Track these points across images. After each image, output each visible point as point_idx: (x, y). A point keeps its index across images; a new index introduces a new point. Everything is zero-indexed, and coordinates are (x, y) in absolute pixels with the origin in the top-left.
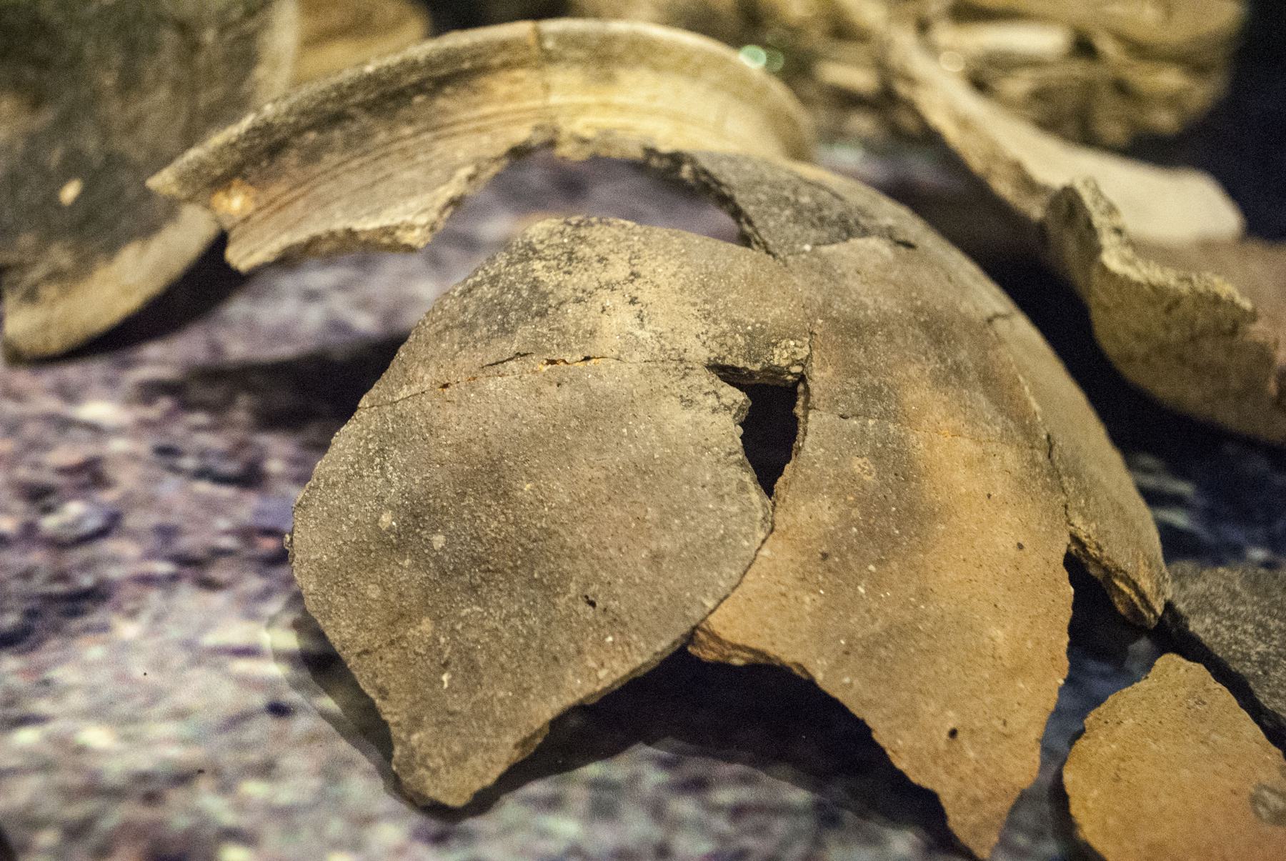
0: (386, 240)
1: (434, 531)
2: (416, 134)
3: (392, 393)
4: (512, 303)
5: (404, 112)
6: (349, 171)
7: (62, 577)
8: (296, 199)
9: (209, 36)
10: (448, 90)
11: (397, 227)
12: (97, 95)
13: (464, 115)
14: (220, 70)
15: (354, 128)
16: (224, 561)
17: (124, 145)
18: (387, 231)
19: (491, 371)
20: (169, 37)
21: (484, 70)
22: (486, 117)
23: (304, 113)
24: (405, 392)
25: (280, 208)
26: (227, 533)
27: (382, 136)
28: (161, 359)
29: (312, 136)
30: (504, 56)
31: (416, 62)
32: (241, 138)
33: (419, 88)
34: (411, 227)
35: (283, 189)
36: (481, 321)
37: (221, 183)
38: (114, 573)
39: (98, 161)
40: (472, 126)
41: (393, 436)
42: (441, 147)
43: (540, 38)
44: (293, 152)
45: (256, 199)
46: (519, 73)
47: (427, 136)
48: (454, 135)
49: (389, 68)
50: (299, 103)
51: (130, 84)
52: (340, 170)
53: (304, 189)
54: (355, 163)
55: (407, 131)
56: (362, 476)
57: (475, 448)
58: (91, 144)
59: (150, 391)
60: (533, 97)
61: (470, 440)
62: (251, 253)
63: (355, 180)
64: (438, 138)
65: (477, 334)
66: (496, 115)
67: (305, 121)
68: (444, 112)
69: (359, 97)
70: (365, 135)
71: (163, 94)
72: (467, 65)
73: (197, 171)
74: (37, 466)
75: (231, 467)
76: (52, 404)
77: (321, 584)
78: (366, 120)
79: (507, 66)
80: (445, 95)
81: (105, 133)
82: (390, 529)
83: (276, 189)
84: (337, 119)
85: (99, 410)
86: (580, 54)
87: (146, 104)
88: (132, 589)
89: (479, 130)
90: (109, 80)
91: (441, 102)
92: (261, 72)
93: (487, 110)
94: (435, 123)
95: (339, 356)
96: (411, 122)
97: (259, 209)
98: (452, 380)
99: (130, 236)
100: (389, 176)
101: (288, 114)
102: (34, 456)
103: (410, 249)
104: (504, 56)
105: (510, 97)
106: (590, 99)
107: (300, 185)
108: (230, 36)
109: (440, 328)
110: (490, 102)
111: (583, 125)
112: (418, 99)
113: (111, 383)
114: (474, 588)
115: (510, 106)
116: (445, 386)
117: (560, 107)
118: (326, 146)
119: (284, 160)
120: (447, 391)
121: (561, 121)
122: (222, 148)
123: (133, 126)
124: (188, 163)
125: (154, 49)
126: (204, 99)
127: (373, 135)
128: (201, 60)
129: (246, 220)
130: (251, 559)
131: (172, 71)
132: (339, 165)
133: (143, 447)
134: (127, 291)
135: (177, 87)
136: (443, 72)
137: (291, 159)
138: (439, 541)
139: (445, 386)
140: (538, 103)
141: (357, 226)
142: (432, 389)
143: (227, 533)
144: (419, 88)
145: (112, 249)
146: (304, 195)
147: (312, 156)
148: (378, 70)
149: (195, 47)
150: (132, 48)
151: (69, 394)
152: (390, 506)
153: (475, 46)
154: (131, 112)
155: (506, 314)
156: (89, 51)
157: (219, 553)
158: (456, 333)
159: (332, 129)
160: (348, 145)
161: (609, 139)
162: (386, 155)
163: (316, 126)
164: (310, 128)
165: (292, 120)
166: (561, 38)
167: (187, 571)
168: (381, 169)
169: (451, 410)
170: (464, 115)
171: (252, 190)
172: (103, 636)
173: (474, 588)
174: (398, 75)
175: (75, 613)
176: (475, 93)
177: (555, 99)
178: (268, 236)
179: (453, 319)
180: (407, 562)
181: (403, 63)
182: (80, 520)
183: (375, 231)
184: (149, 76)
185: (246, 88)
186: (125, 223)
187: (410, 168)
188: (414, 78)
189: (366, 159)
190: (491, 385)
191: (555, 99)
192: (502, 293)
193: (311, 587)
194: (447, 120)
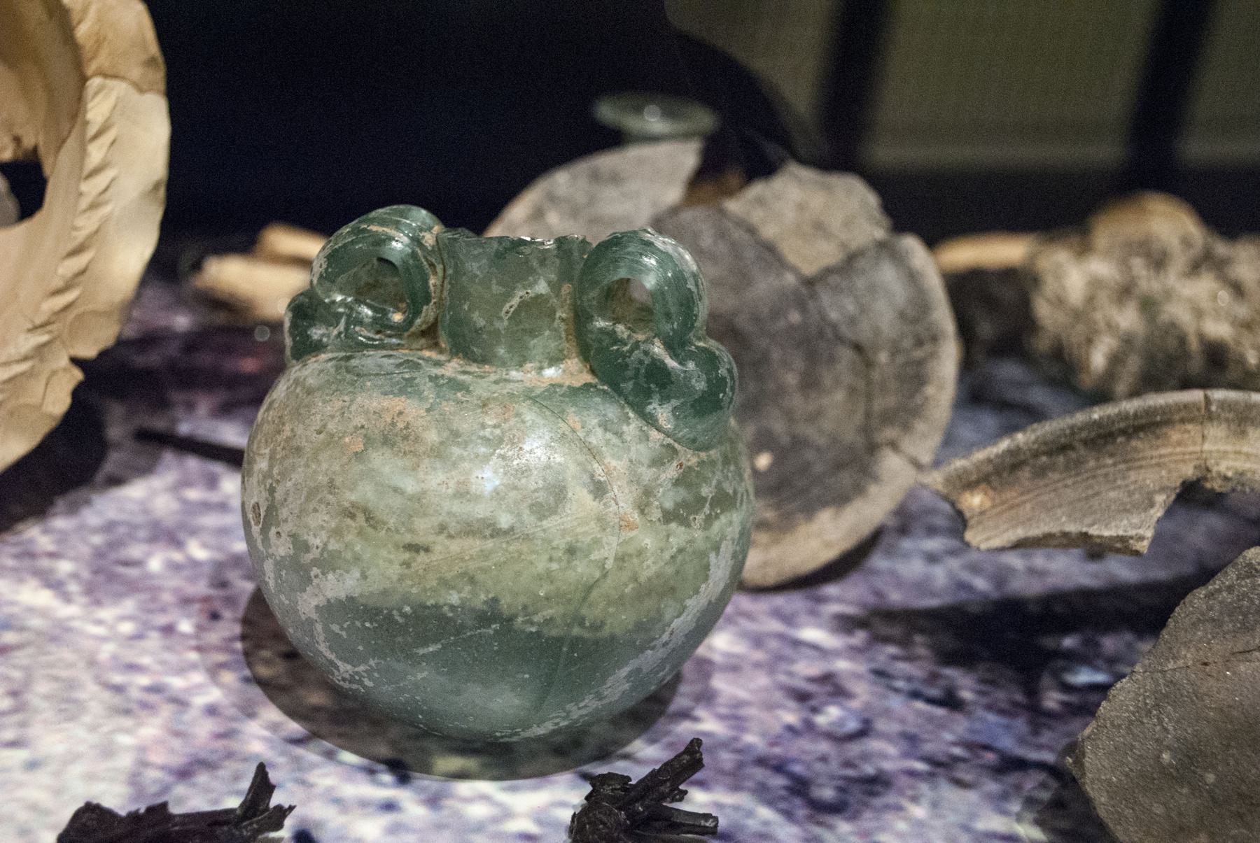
0: (1118, 545)
1: (1206, 769)
2: (1115, 465)
3: (1161, 664)
4: (1249, 608)
5: (1110, 448)
6: (1066, 486)
7: (848, 764)
8: (1024, 502)
9: (883, 357)
10: (1142, 435)
11: (1132, 538)
12: (781, 391)
13: (1148, 453)
14: (893, 384)
15: (1073, 455)
16: (962, 766)
17: (809, 431)
18: (1122, 539)
19: (1240, 657)
20: (846, 355)
21: (1168, 422)
22: (1161, 456)
23: (1045, 443)
24: (1171, 665)
25: (1012, 507)
26: (955, 744)
27: (1092, 463)
28: (843, 597)
29: (1044, 459)
30: (1183, 414)
31: (1128, 413)
32: (997, 456)
33: (1123, 432)
34: (1141, 538)
35: (1014, 494)
36: (1226, 619)
37: (971, 486)
38: (888, 766)
39: (785, 440)
40: (1154, 461)
41: (1166, 696)
42: (1133, 475)
43: (1208, 401)
44: (1028, 469)
45: (993, 499)
46: (1189, 427)
47: (1122, 466)
48: (1141, 467)
49: (1109, 417)
50: (1044, 436)
51: (810, 384)
52: (1060, 485)
53: (1031, 495)
54: (1069, 482)
55: (1110, 461)
56: (1142, 723)
57: (1235, 713)
58: (778, 426)
59: (846, 624)
60: (1194, 443)
61: (1230, 706)
62: (988, 539)
63: (1070, 494)
64: (1129, 469)
65: (1225, 628)
66: (1171, 454)
67: (1044, 448)
68: (1136, 450)
69: (1084, 435)
70: (1079, 462)
71: (840, 396)
72: (1158, 418)
73: (959, 477)
74: (790, 674)
75: (934, 692)
76: (776, 626)
77: (1111, 798)
78: (1082, 451)
79: (1183, 421)
80: (1139, 438)
81: (789, 416)
82: (1170, 765)
83: (1010, 494)
84: (1064, 448)
85: (812, 634)
86: (1231, 416)
87: (825, 401)
88: (904, 781)
89: (1158, 465)
90: (791, 379)
91: (1134, 443)
92: (930, 390)
93: (1163, 451)
94: (1129, 457)
95: (974, 609)
96: (1112, 455)
97: (993, 507)
98: (1211, 660)
99: (824, 504)
100: (1097, 494)
101: (1034, 443)
102: (783, 666)
103: (1137, 553)
104: (1183, 414)
105: (1179, 444)
106: (1229, 448)
107: (1029, 492)
108: (900, 359)
109: (1194, 620)
110: (1164, 445)
111: (1225, 467)
112: (1120, 440)
113: (813, 613)
114: (1240, 816)
115: (1178, 450)
116: (1206, 664)
117: (1211, 452)
118: (1052, 467)
119: (1020, 473)
120: (1208, 669)
121: (1211, 462)
122: (982, 462)
123: (814, 417)
124: (956, 470)
125: (832, 360)
126: (879, 404)
127: (1086, 462)
128: (876, 375)
129: (982, 513)
130: (982, 766)
131: (847, 378)
132: (1059, 481)
133: (861, 667)
134: (828, 545)
135: (852, 391)
136: (1143, 421)
137: (1025, 473)
138: (1211, 778)
139: (1206, 664)
140: (1198, 448)
141: (1093, 531)
142: (1194, 665)
143: (955, 744)
144: (1123, 432)
145: (809, 511)
146: (1030, 500)
147: (1041, 472)
148: (1101, 418)
149: (869, 364)
150: (812, 357)
151: (789, 619)
152: (1168, 748)
153: (1168, 406)
154: (811, 407)
155: (1245, 616)
156: (776, 355)
157: (956, 759)
158: (1208, 626)
159: (1058, 454)
160: (1067, 468)
161: (1244, 479)
162: (1094, 477)
163: (1049, 453)
164: (1044, 453)
165: (1036, 446)
166: (1223, 404)
167: (939, 770)
168: (1091, 487)
169: (1212, 682)
170: (1148, 453)
171: (991, 493)
172: (901, 814)
173: (1240, 816)
174: (1113, 422)
175: (873, 794)
176: (1158, 438)
177: (1207, 447)
178: (1002, 527)
179: (1203, 614)
180: (1185, 791)
181: (1120, 413)
182: (841, 722)
183: (1111, 538)
184: (828, 381)
185: (918, 400)
186: (816, 491)
187: (1114, 489)
188: (1122, 425)
189: (1079, 479)
190: (1242, 668)
191: (1207, 447)
192: (1239, 600)
193: (1103, 799)
194: (1136, 456)
